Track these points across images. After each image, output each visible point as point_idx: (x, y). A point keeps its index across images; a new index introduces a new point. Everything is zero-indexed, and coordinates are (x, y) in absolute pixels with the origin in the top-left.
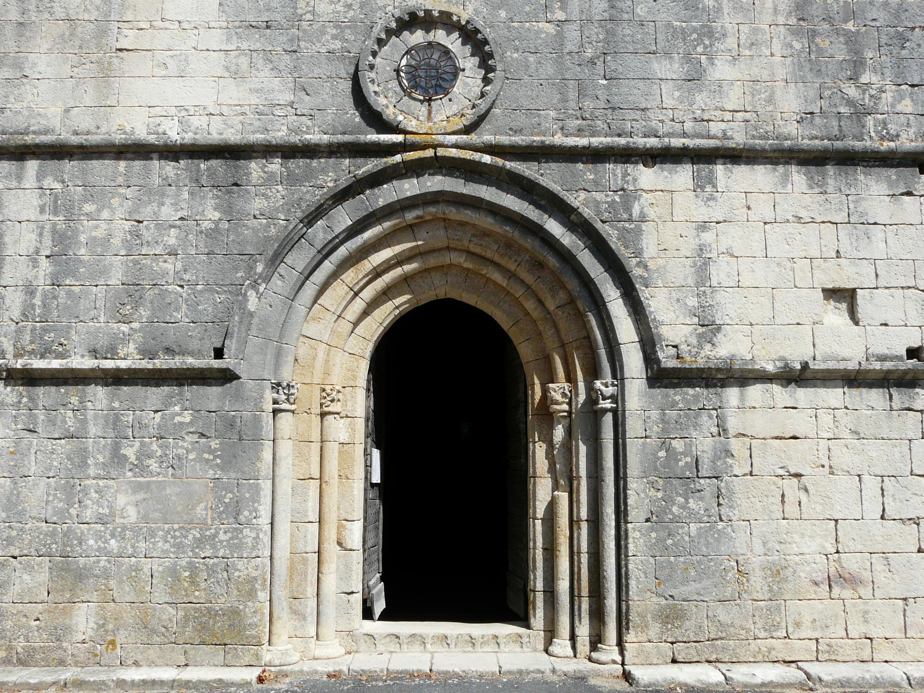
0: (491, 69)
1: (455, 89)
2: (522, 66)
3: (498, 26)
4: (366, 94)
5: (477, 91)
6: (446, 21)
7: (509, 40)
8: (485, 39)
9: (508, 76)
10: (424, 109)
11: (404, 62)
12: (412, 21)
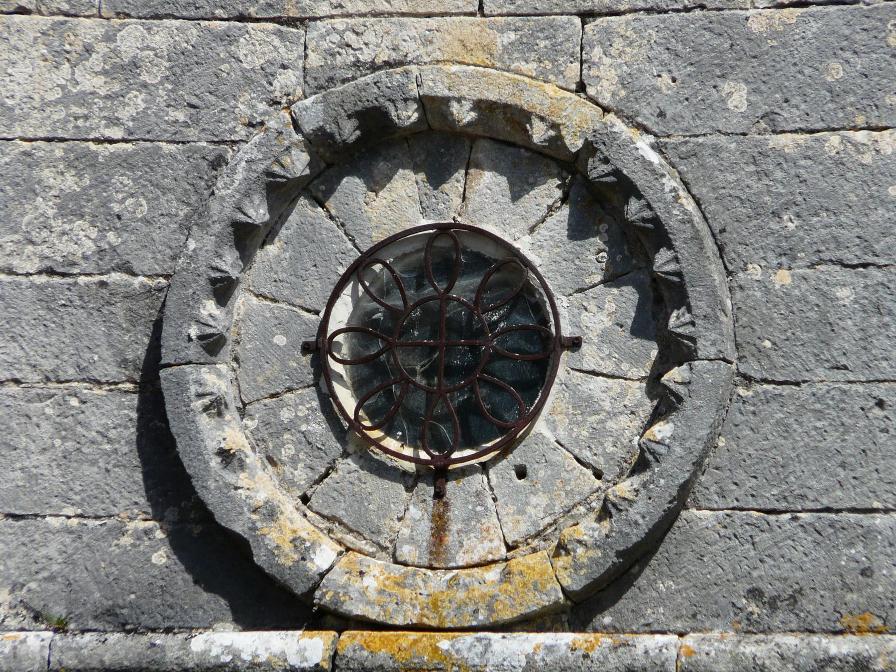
0: (676, 351)
1: (540, 426)
2: (808, 325)
3: (716, 150)
4: (191, 466)
5: (627, 428)
6: (504, 139)
7: (758, 209)
8: (656, 220)
9: (753, 368)
10: (411, 514)
11: (342, 313)
12: (366, 143)
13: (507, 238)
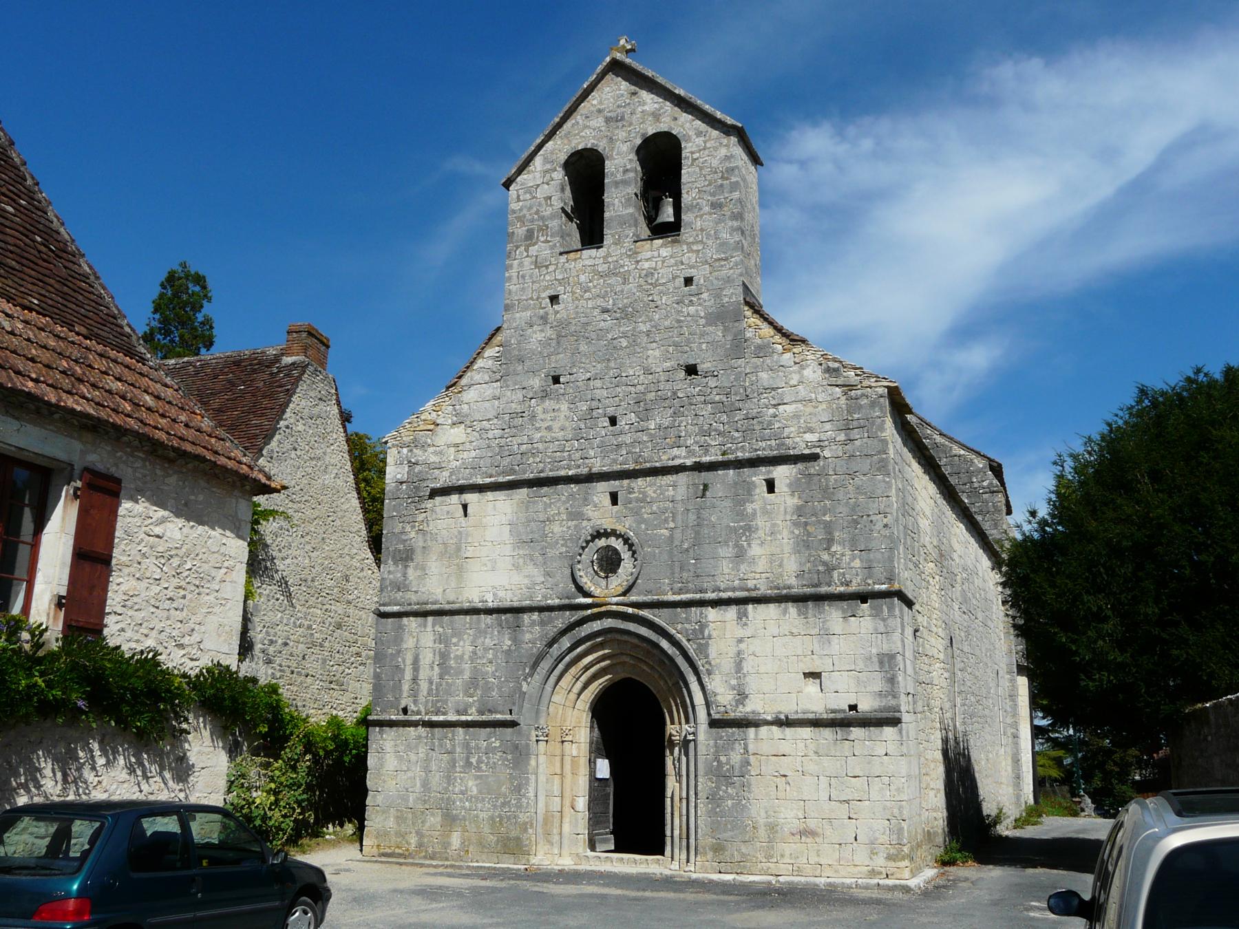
6: (613, 533)
10: (604, 582)
12: (598, 535)
13: (668, 86)
